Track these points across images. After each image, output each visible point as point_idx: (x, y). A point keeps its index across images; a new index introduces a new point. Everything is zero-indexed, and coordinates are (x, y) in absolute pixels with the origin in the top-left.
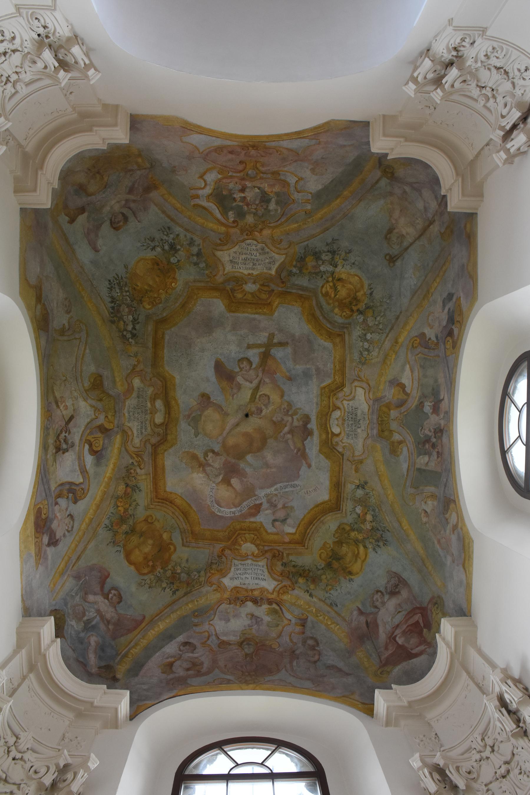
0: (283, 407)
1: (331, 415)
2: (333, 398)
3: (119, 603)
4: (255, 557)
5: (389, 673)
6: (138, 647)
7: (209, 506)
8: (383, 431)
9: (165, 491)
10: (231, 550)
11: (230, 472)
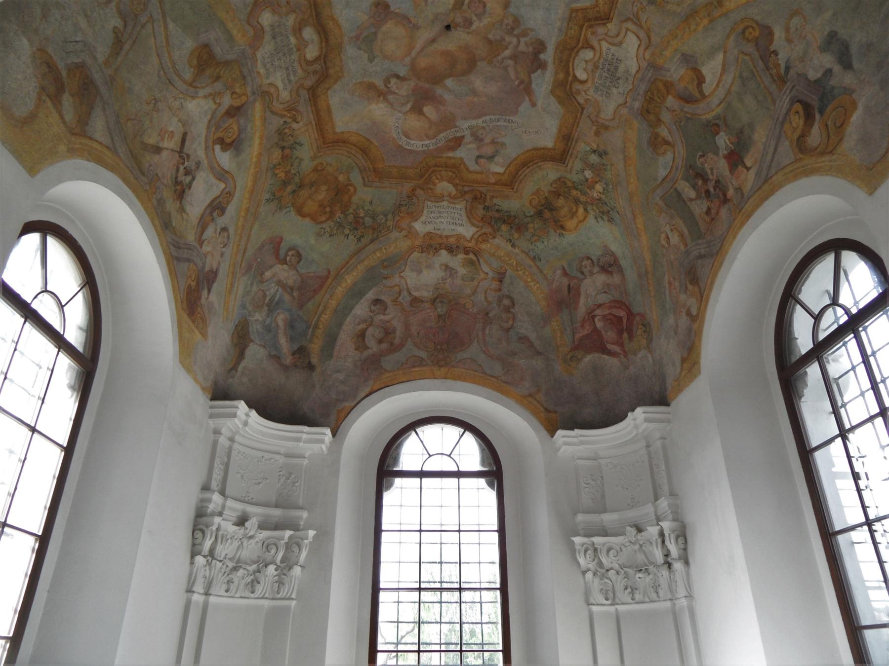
0: (506, 21)
1: (578, 52)
2: (586, 30)
3: (299, 262)
4: (453, 198)
5: (579, 360)
6: (328, 312)
7: (394, 139)
8: (649, 111)
9: (335, 133)
10: (423, 189)
11: (422, 99)
